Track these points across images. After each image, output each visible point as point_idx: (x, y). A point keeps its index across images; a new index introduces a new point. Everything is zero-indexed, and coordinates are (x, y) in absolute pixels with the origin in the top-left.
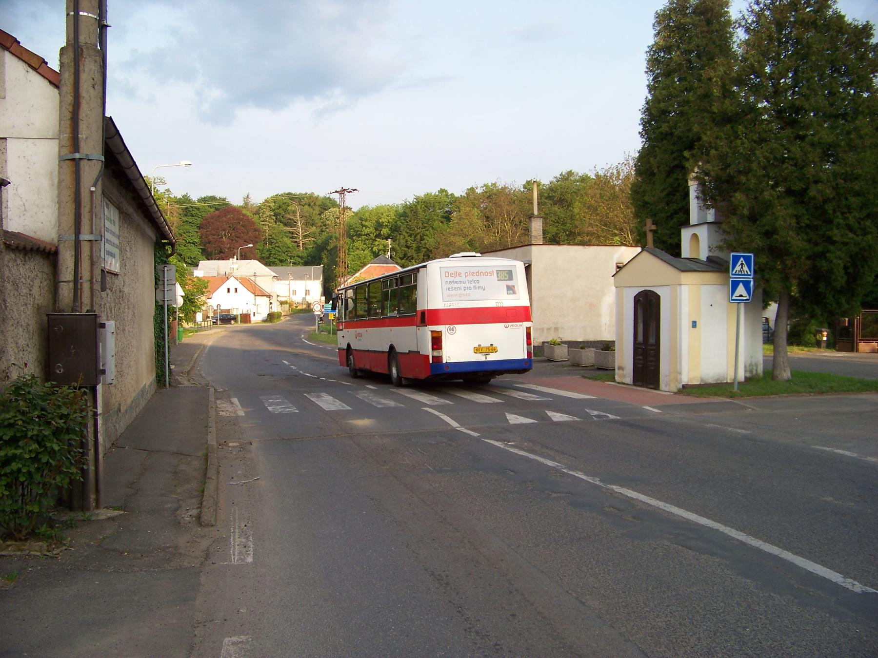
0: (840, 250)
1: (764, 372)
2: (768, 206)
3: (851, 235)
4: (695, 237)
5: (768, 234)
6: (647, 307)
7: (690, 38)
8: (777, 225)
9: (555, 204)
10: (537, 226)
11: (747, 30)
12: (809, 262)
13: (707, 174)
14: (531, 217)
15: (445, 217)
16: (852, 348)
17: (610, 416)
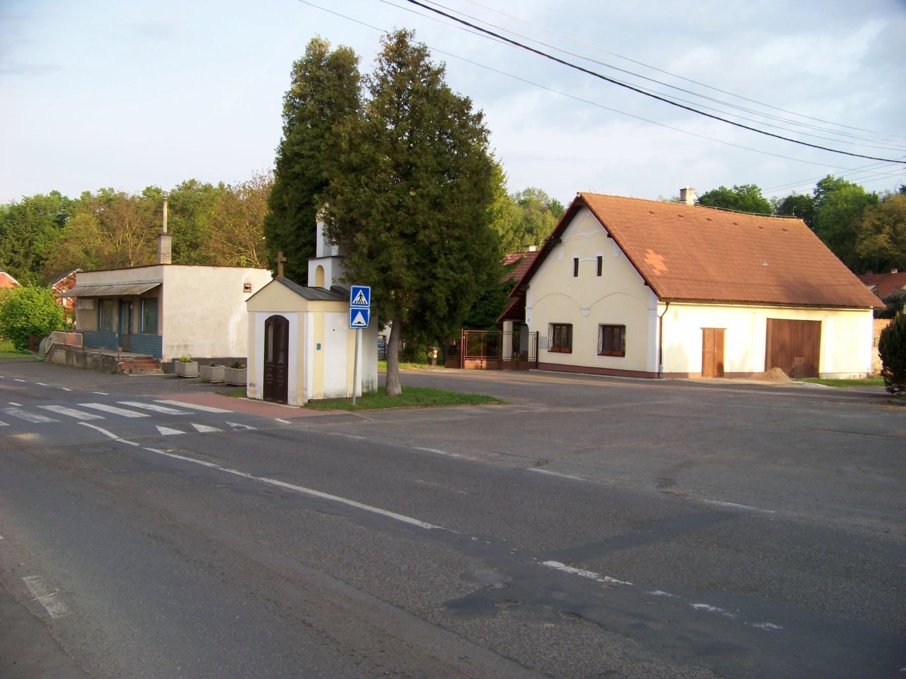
0: (443, 285)
1: (379, 388)
2: (385, 246)
3: (451, 273)
5: (384, 270)
6: (277, 330)
7: (323, 89)
8: (391, 263)
9: (176, 213)
10: (166, 244)
11: (374, 91)
12: (417, 295)
13: (333, 215)
14: (160, 235)
15: (57, 222)
16: (459, 365)
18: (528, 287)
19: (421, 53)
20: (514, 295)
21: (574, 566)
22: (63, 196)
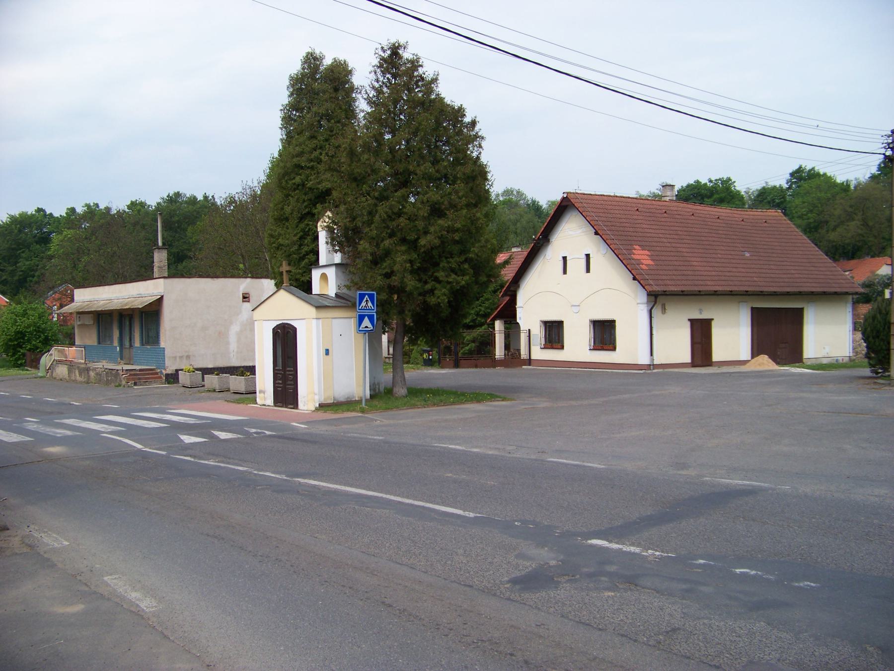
3: (453, 276)
4: (324, 277)
11: (370, 102)
17: (268, 433)
18: (519, 287)
19: (415, 64)
20: (505, 295)
21: (617, 543)
22: (48, 212)
